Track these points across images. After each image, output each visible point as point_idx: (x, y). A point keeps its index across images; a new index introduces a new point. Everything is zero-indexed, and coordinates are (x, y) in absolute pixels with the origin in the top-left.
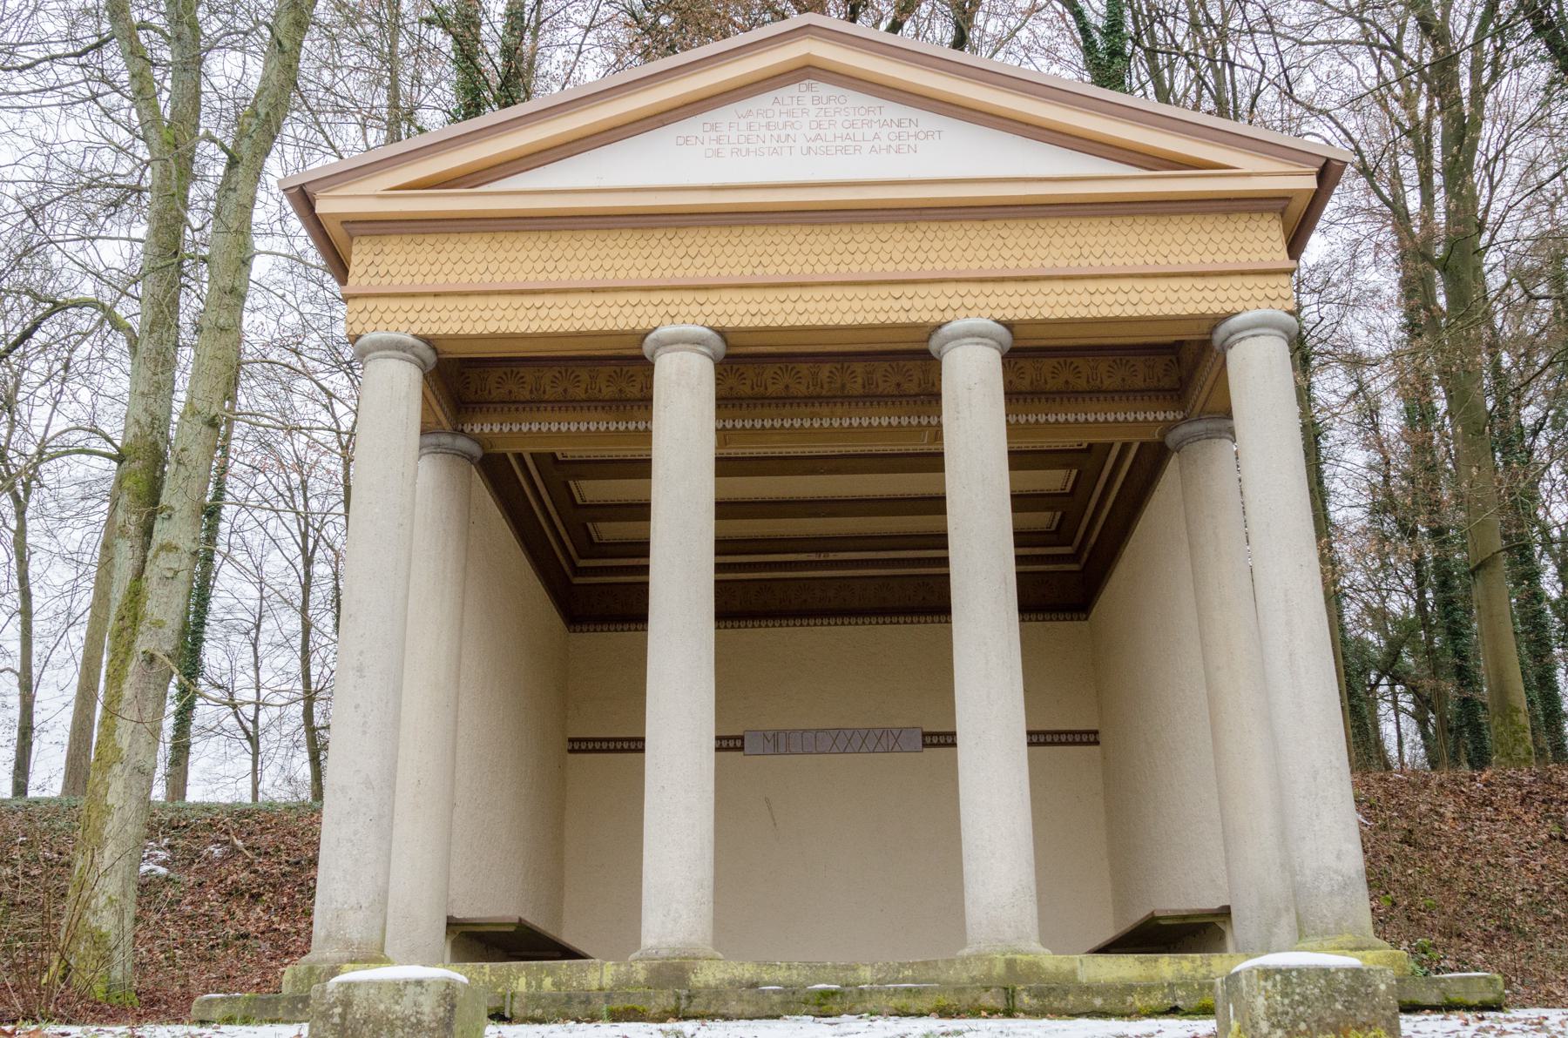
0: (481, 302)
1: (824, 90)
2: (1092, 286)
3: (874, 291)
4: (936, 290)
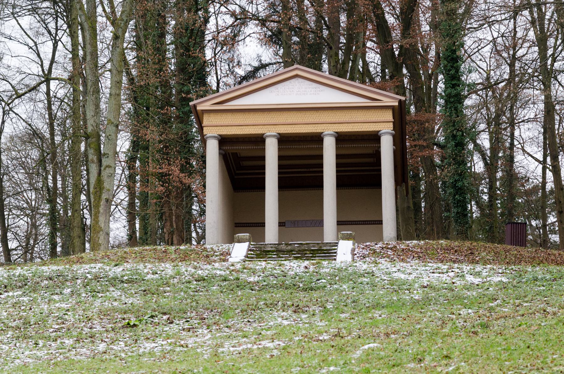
0: (231, 127)
1: (300, 80)
2: (353, 124)
3: (310, 125)
4: (322, 125)
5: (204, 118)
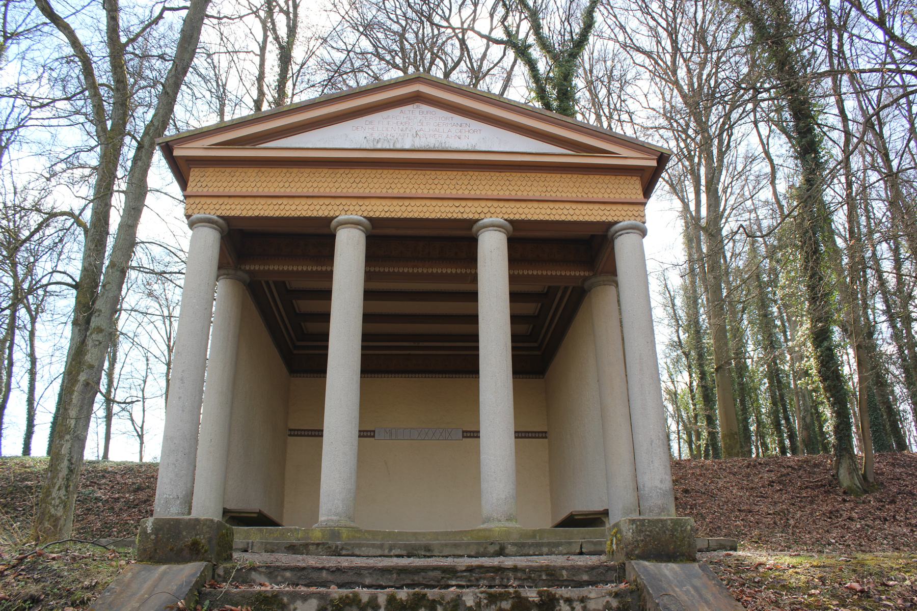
0: (251, 201)
1: (425, 108)
2: (552, 205)
3: (446, 203)
4: (476, 203)
5: (191, 174)
